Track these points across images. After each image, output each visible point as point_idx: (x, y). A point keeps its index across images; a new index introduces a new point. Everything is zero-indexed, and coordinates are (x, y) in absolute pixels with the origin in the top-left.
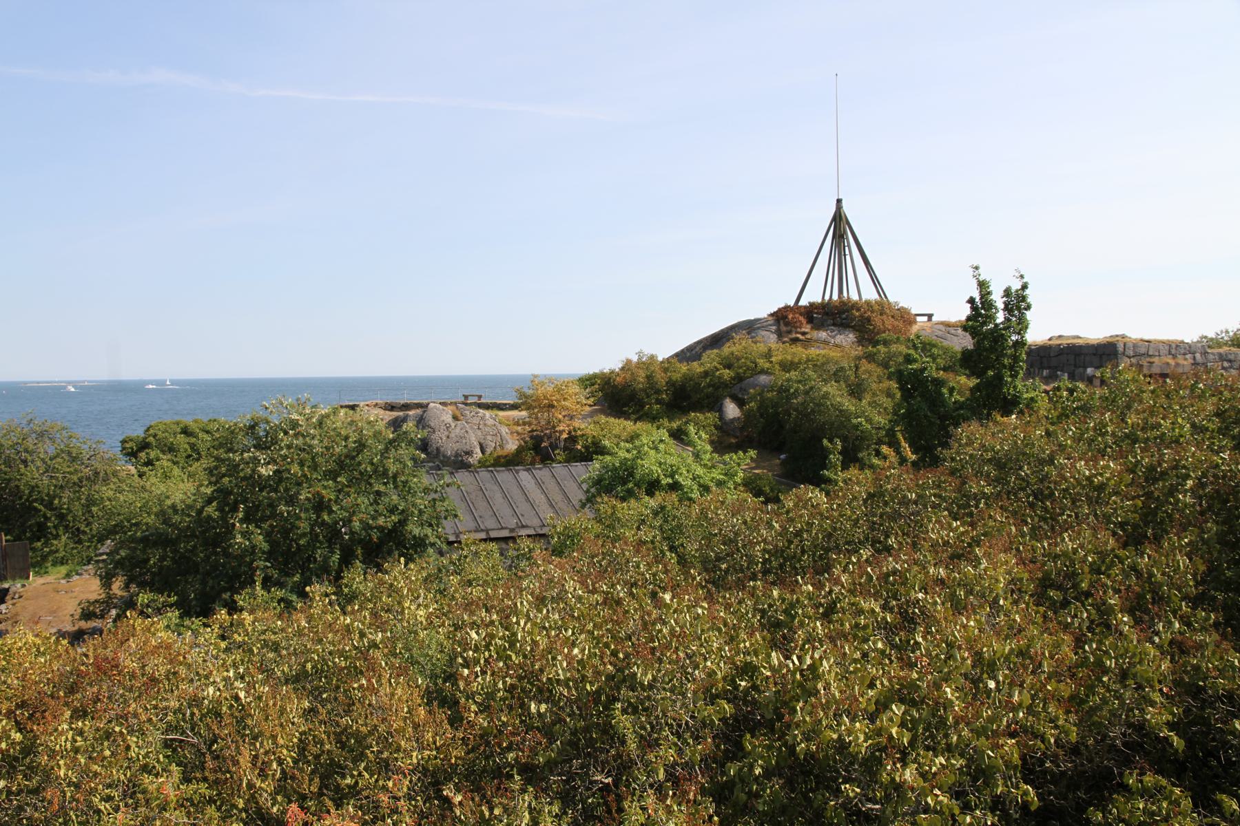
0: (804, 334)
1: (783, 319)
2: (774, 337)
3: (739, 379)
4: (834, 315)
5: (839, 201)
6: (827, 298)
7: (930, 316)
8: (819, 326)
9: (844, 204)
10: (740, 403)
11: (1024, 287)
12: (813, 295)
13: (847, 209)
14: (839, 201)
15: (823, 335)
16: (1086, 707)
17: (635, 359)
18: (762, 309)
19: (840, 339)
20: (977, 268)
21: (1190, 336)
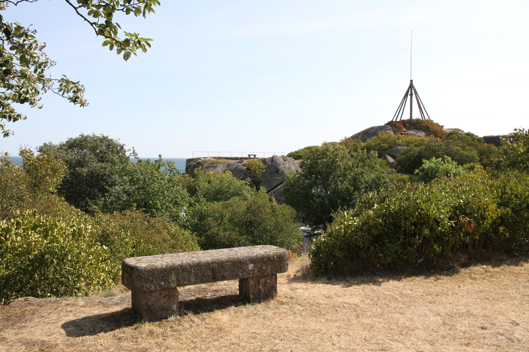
0: (404, 131)
1: (392, 124)
2: (392, 133)
3: (390, 147)
4: (413, 124)
5: (411, 81)
6: (394, 120)
7: (255, 156)
8: (409, 129)
9: (413, 82)
10: (393, 157)
11: (160, 156)
12: (406, 116)
13: (414, 84)
14: (411, 81)
15: (412, 132)
16: (418, 241)
17: (344, 139)
18: (382, 122)
19: (419, 134)
20: (6, 135)
21: (481, 131)
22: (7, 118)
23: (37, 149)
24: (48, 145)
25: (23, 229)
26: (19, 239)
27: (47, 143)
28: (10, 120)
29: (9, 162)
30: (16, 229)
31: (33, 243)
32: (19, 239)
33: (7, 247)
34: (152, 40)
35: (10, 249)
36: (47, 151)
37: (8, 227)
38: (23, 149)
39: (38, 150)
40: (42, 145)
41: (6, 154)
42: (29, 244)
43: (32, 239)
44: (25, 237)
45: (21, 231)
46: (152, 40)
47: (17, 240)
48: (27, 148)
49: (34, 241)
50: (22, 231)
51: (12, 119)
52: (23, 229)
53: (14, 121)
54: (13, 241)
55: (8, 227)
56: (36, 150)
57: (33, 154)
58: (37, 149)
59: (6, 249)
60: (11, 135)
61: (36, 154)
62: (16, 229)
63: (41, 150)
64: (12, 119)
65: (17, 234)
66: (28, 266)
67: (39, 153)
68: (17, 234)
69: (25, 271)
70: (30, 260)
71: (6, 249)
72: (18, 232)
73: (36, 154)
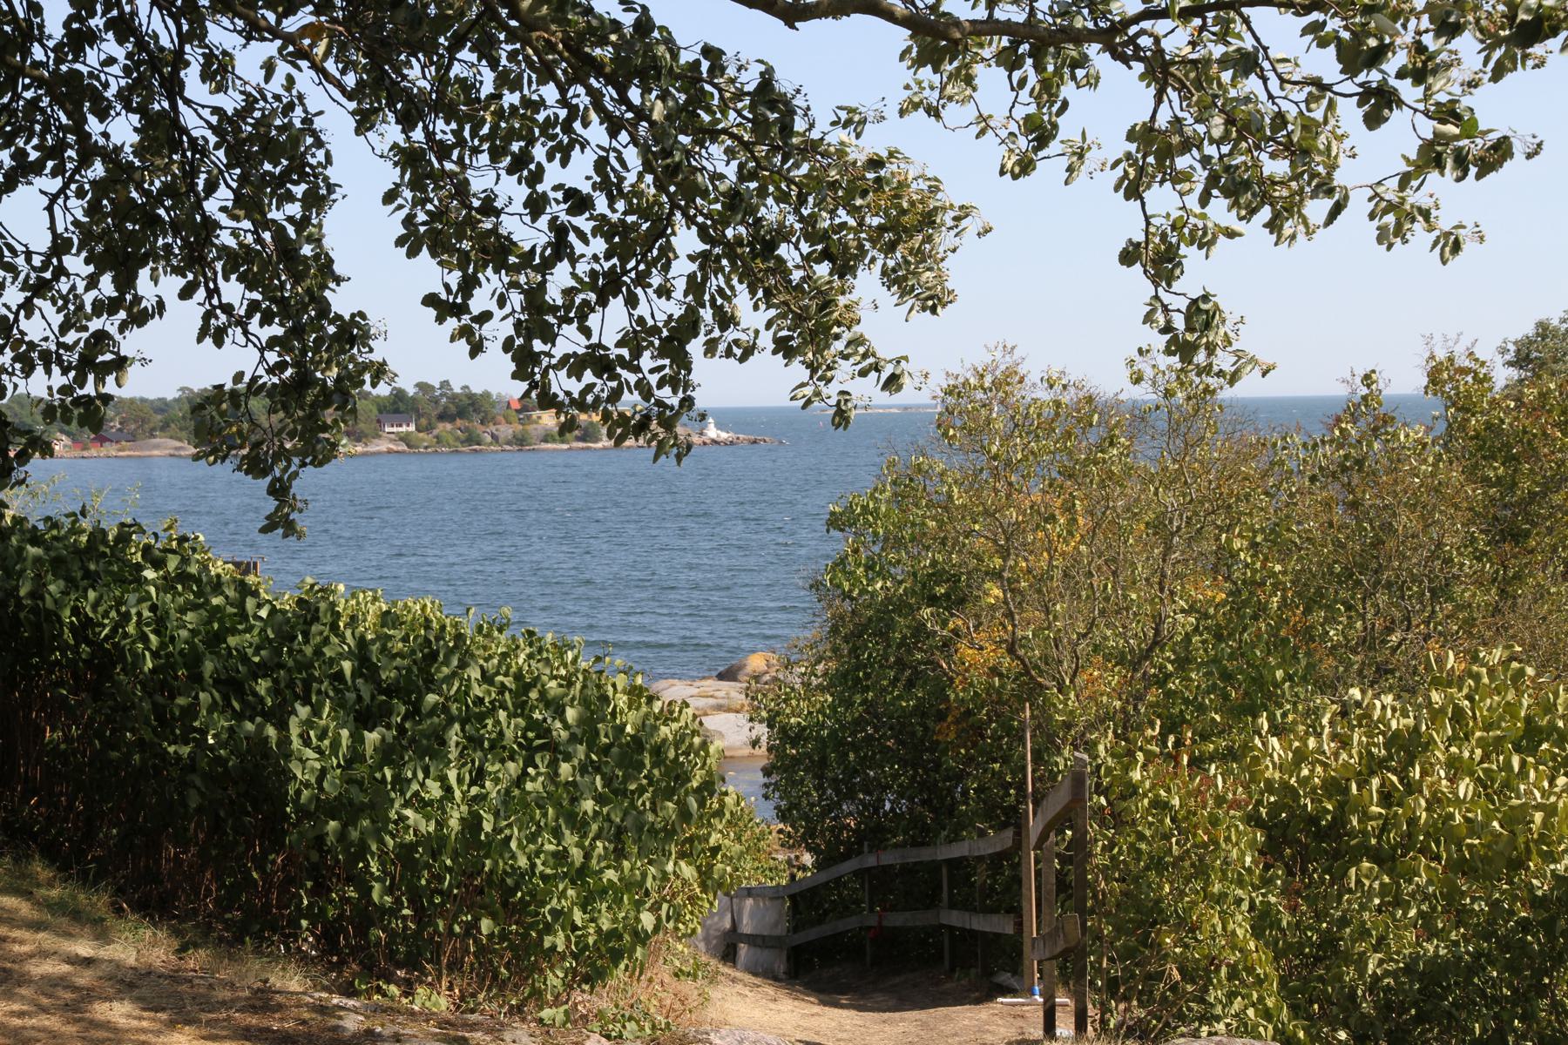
20: (1451, 245)
22: (1449, 163)
23: (1504, 351)
24: (1556, 330)
25: (1481, 743)
26: (1465, 787)
27: (1555, 322)
28: (1465, 172)
29: (1387, 420)
30: (1451, 741)
31: (1538, 817)
32: (1465, 787)
33: (1412, 822)
34: (1404, 157)
35: (1427, 835)
36: (1556, 361)
37: (1416, 728)
38: (1441, 355)
39: (1510, 357)
40: (1529, 330)
41: (1367, 379)
42: (1516, 819)
43: (1529, 793)
44: (1494, 788)
45: (1470, 752)
46: (1404, 157)
47: (1456, 794)
48: (1460, 350)
49: (1538, 807)
50: (1478, 752)
51: (1473, 170)
52: (1481, 743)
53: (1479, 177)
54: (1435, 801)
55: (1416, 728)
56: (1499, 360)
57: (1487, 378)
58: (1504, 351)
59: (1410, 835)
60: (1468, 247)
61: (1503, 376)
62: (1451, 741)
63: (1523, 357)
64: (1473, 170)
65: (1456, 768)
66: (1524, 925)
67: (1514, 373)
68: (1456, 768)
69: (1513, 952)
70: (1536, 903)
71: (1410, 835)
72: (1459, 758)
73: (1503, 376)
